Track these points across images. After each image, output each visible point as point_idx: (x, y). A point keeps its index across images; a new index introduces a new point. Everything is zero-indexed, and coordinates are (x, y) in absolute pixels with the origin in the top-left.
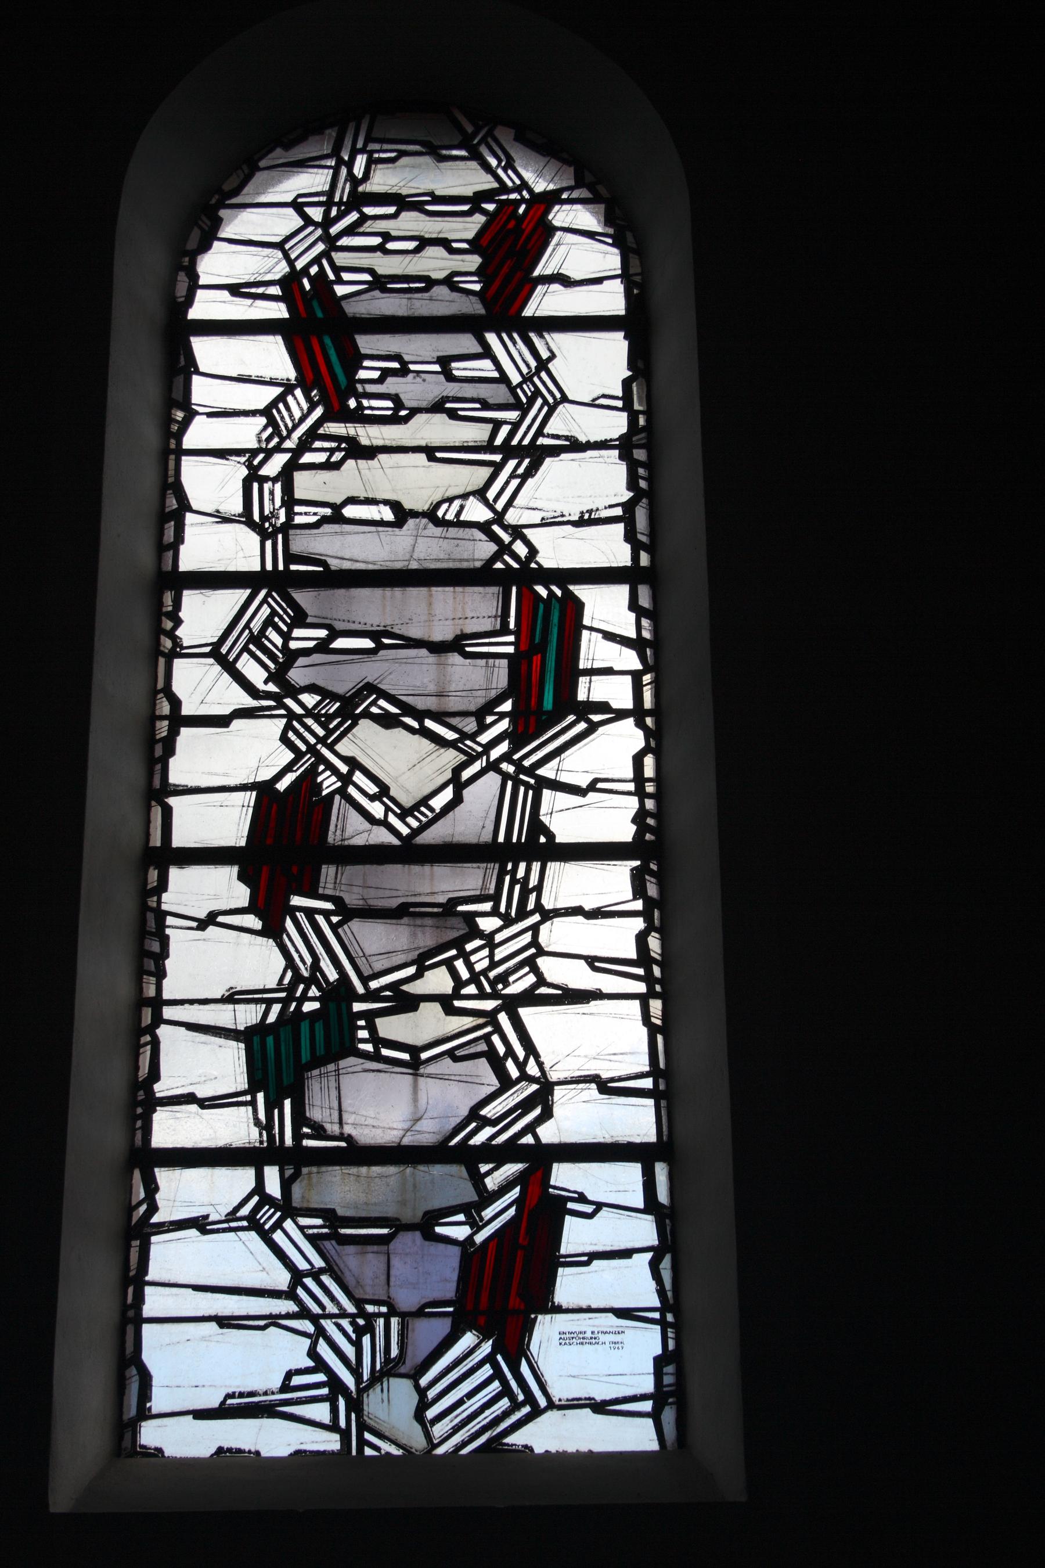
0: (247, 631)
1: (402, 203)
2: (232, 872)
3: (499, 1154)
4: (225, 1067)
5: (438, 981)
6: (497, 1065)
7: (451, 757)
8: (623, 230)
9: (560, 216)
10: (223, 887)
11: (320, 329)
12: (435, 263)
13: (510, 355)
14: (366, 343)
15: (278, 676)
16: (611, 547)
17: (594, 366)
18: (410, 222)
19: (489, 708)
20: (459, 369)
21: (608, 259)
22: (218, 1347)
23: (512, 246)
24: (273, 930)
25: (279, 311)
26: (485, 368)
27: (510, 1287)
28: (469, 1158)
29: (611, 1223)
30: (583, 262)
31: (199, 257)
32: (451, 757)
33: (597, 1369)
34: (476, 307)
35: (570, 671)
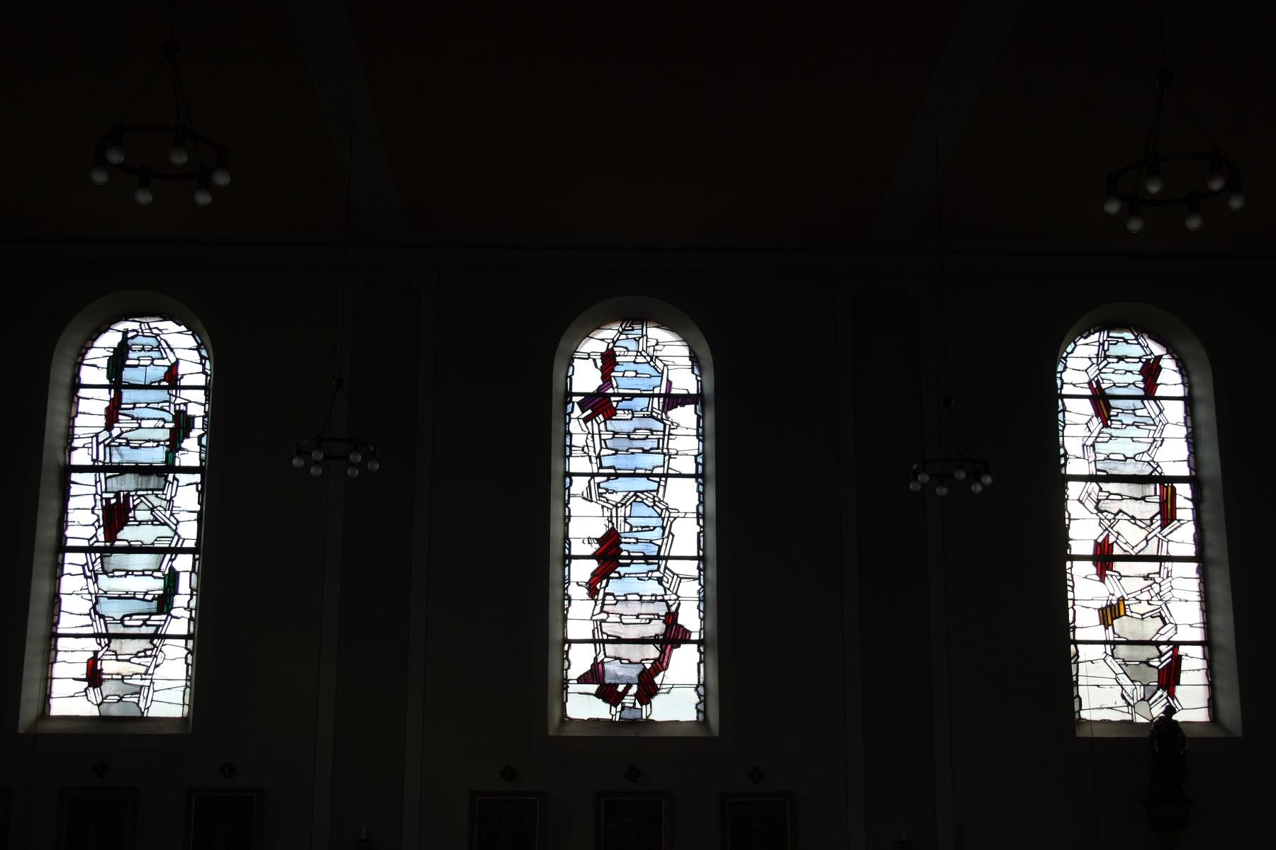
0: (652, 652)
1: (1120, 358)
2: (1090, 563)
3: (1168, 643)
4: (1095, 617)
5: (1145, 596)
6: (1163, 619)
7: (1144, 533)
8: (1183, 369)
9: (1163, 363)
10: (1089, 568)
11: (1101, 400)
12: (1130, 378)
13: (1151, 404)
14: (1113, 403)
15: (1096, 508)
16: (1184, 471)
17: (1176, 411)
18: (1122, 365)
19: (1152, 519)
20: (1138, 412)
21: (1177, 378)
22: (1103, 694)
23: (1151, 371)
24: (1102, 580)
25: (1089, 392)
26: (1144, 412)
27: (1170, 677)
28: (1157, 644)
29: (1193, 663)
30: (1170, 380)
31: (1188, 735)
32: (1144, 533)
33: (1192, 703)
34: (1141, 393)
35: (1174, 508)
